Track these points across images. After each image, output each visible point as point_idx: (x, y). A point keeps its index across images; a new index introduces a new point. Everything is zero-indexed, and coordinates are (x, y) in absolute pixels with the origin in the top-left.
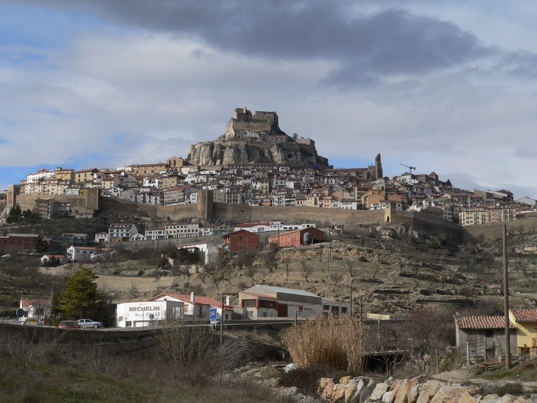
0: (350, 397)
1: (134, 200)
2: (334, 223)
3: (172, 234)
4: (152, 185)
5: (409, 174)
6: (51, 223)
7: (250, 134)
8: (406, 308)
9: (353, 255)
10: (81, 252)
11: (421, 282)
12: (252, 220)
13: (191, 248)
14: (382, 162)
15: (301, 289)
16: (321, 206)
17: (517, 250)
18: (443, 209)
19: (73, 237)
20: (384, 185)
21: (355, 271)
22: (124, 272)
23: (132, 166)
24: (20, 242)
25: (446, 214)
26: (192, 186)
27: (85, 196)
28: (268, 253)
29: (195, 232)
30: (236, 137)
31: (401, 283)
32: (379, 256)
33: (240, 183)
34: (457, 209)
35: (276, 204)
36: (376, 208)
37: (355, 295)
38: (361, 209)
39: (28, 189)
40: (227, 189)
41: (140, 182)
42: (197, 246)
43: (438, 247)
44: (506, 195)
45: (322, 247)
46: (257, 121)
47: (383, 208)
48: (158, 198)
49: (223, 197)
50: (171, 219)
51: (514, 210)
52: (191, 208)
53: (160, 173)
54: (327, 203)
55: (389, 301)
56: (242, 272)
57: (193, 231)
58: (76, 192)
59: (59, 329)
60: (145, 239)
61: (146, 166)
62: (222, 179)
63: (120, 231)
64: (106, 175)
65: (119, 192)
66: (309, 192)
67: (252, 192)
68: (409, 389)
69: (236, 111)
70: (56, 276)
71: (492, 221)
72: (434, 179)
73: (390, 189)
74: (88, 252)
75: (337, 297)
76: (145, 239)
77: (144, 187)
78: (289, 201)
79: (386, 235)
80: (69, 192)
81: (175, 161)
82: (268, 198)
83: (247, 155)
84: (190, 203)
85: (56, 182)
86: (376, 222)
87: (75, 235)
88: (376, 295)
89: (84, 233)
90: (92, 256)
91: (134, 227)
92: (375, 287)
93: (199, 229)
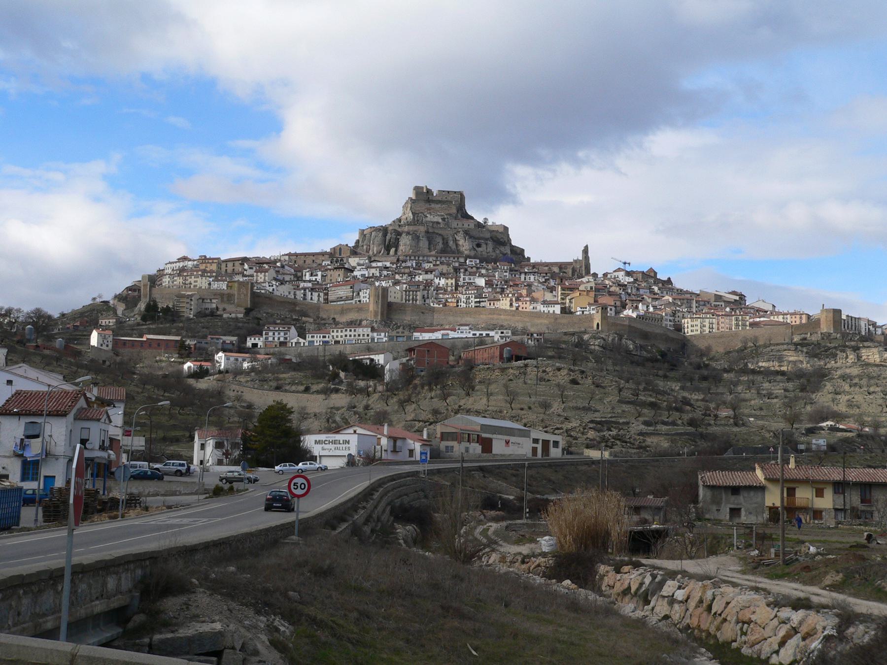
0: (638, 589)
2: (532, 330)
3: (339, 339)
5: (623, 270)
6: (195, 322)
7: (430, 218)
8: (626, 442)
9: (563, 377)
10: (232, 359)
11: (645, 411)
13: (365, 358)
15: (504, 418)
16: (517, 309)
17: (750, 365)
20: (593, 285)
21: (567, 397)
22: (287, 388)
23: (290, 255)
25: (666, 320)
27: (235, 291)
28: (462, 371)
29: (366, 337)
30: (417, 220)
34: (680, 314)
37: (569, 426)
38: (566, 313)
39: (166, 280)
40: (405, 286)
41: (299, 274)
42: (372, 357)
43: (657, 361)
44: (737, 298)
45: (526, 366)
47: (594, 312)
48: (322, 294)
49: (399, 296)
51: (748, 317)
54: (524, 306)
55: (606, 433)
56: (433, 394)
58: (223, 286)
60: (307, 344)
62: (399, 274)
63: (276, 334)
65: (274, 287)
66: (503, 290)
68: (704, 592)
70: (207, 390)
73: (600, 290)
74: (240, 359)
75: (546, 427)
78: (479, 302)
79: (595, 345)
80: (215, 286)
82: (453, 297)
83: (427, 243)
86: (583, 329)
87: (224, 338)
88: (591, 425)
89: (233, 336)
90: (246, 365)
91: (293, 331)
92: (590, 416)
93: (370, 334)
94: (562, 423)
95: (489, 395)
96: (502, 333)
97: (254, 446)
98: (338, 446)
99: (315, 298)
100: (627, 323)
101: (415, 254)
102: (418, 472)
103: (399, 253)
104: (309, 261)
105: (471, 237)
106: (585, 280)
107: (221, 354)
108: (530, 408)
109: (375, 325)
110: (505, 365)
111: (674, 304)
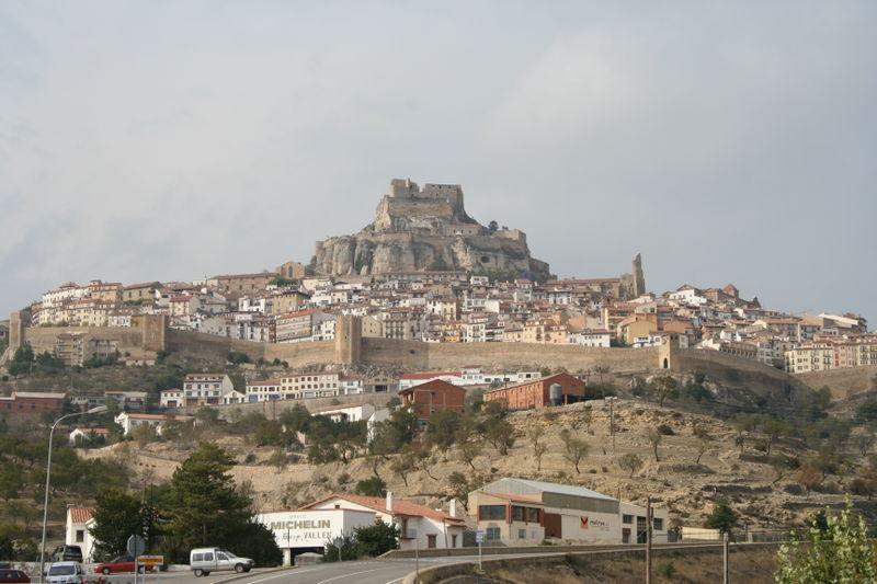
1: (225, 335)
3: (293, 391)
4: (254, 309)
7: (416, 222)
12: (430, 367)
14: (644, 267)
18: (758, 345)
19: (124, 399)
23: (219, 278)
24: (34, 407)
25: (762, 353)
26: (324, 310)
29: (331, 388)
30: (396, 228)
31: (746, 472)
32: (694, 424)
33: (405, 304)
35: (470, 340)
36: (642, 344)
37: (673, 495)
39: (44, 317)
40: (385, 315)
41: (233, 304)
42: (344, 411)
43: (753, 411)
44: (856, 323)
46: (426, 200)
48: (266, 330)
50: (290, 365)
52: (323, 346)
53: (268, 289)
56: (448, 455)
57: (328, 385)
58: (125, 321)
59: (16, 528)
60: (246, 400)
61: (241, 278)
62: (375, 298)
63: (203, 386)
64: (177, 292)
67: (427, 320)
69: (392, 184)
71: (841, 365)
72: (731, 297)
75: (636, 498)
76: (246, 400)
77: (241, 313)
80: (114, 322)
81: (291, 268)
84: (321, 338)
85: (92, 305)
88: (707, 494)
89: (141, 391)
91: (227, 381)
92: (701, 482)
93: (338, 383)
94: (661, 491)
95: (540, 451)
96: (528, 376)
97: (166, 527)
98: (311, 530)
99: (257, 335)
100: (707, 358)
101: (397, 270)
102: (471, 565)
103: (374, 272)
104: (247, 285)
105: (473, 247)
106: (640, 300)
107: (123, 416)
108: (605, 470)
109: (345, 372)
110: (555, 409)
111: (771, 331)
